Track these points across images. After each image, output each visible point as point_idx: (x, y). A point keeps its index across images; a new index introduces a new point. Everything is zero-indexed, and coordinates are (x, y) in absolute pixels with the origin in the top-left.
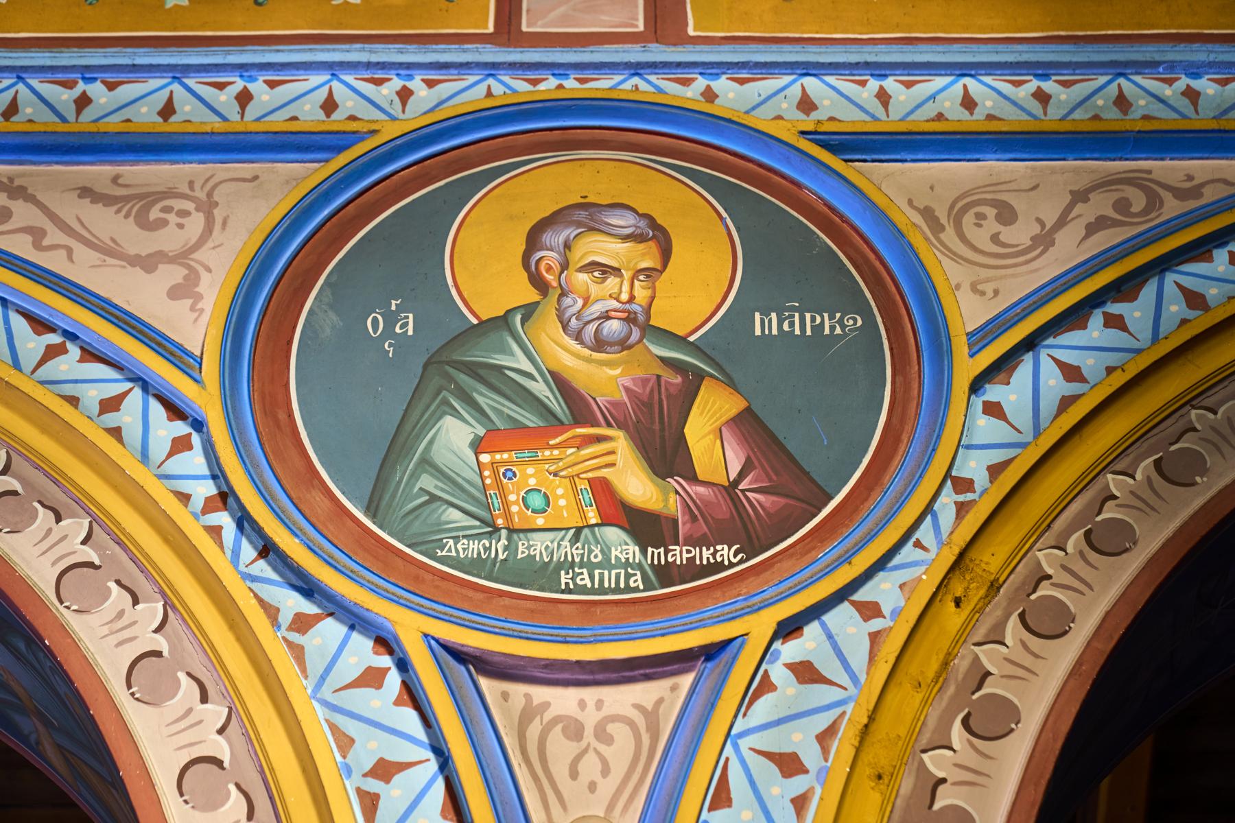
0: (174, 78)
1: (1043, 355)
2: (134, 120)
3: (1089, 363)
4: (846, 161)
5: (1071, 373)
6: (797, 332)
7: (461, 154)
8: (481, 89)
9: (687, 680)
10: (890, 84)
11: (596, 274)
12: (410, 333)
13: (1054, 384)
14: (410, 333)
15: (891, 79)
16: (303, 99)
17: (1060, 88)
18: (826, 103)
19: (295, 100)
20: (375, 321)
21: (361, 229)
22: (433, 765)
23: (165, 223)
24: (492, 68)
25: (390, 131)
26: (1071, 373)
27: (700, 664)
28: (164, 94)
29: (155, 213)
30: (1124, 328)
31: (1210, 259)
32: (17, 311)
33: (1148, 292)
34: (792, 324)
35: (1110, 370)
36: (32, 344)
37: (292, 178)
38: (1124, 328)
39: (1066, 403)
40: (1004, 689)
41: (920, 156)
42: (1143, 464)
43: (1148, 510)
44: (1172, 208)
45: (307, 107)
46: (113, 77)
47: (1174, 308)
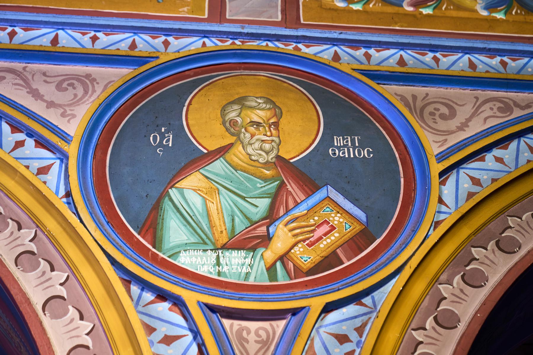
0: (134, 33)
1: (461, 171)
2: (121, 49)
3: (484, 177)
4: (378, 84)
5: (476, 182)
6: (347, 156)
7: (199, 71)
8: (200, 43)
9: (282, 324)
10: (372, 51)
11: (255, 126)
12: (170, 145)
13: (466, 185)
14: (170, 145)
15: (506, 57)
16: (44, 37)
17: (104, 35)
18: (480, 67)
19: (118, 42)
20: (155, 138)
21: (148, 97)
22: (190, 337)
23: (66, 89)
24: (205, 34)
25: (163, 59)
26: (476, 182)
27: (289, 316)
28: (131, 40)
29: (65, 85)
30: (472, 178)
31: (483, 160)
32: (6, 122)
33: (514, 145)
34: (344, 153)
35: (494, 180)
36: (10, 137)
37: (123, 73)
38: (472, 178)
39: (471, 195)
40: (428, 349)
41: (411, 84)
42: (492, 242)
43: (461, 301)
44: (517, 113)
45: (45, 40)
46: (28, 25)
47: (466, 186)
